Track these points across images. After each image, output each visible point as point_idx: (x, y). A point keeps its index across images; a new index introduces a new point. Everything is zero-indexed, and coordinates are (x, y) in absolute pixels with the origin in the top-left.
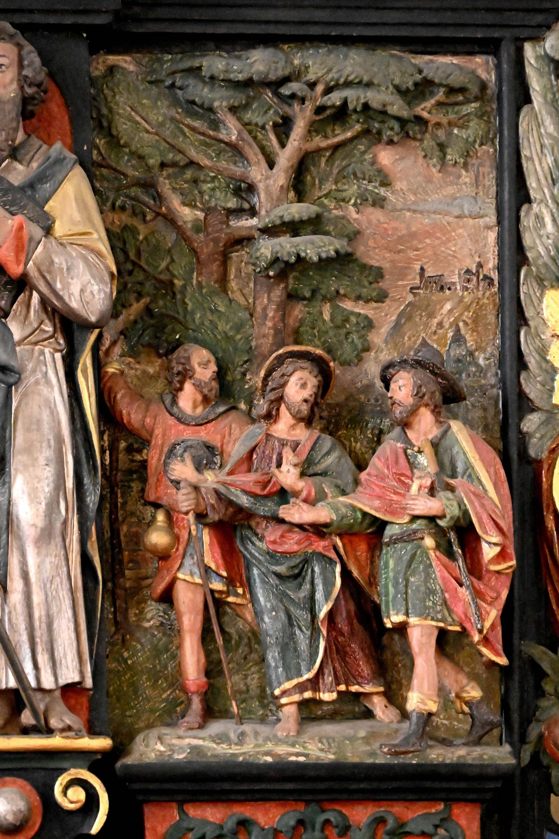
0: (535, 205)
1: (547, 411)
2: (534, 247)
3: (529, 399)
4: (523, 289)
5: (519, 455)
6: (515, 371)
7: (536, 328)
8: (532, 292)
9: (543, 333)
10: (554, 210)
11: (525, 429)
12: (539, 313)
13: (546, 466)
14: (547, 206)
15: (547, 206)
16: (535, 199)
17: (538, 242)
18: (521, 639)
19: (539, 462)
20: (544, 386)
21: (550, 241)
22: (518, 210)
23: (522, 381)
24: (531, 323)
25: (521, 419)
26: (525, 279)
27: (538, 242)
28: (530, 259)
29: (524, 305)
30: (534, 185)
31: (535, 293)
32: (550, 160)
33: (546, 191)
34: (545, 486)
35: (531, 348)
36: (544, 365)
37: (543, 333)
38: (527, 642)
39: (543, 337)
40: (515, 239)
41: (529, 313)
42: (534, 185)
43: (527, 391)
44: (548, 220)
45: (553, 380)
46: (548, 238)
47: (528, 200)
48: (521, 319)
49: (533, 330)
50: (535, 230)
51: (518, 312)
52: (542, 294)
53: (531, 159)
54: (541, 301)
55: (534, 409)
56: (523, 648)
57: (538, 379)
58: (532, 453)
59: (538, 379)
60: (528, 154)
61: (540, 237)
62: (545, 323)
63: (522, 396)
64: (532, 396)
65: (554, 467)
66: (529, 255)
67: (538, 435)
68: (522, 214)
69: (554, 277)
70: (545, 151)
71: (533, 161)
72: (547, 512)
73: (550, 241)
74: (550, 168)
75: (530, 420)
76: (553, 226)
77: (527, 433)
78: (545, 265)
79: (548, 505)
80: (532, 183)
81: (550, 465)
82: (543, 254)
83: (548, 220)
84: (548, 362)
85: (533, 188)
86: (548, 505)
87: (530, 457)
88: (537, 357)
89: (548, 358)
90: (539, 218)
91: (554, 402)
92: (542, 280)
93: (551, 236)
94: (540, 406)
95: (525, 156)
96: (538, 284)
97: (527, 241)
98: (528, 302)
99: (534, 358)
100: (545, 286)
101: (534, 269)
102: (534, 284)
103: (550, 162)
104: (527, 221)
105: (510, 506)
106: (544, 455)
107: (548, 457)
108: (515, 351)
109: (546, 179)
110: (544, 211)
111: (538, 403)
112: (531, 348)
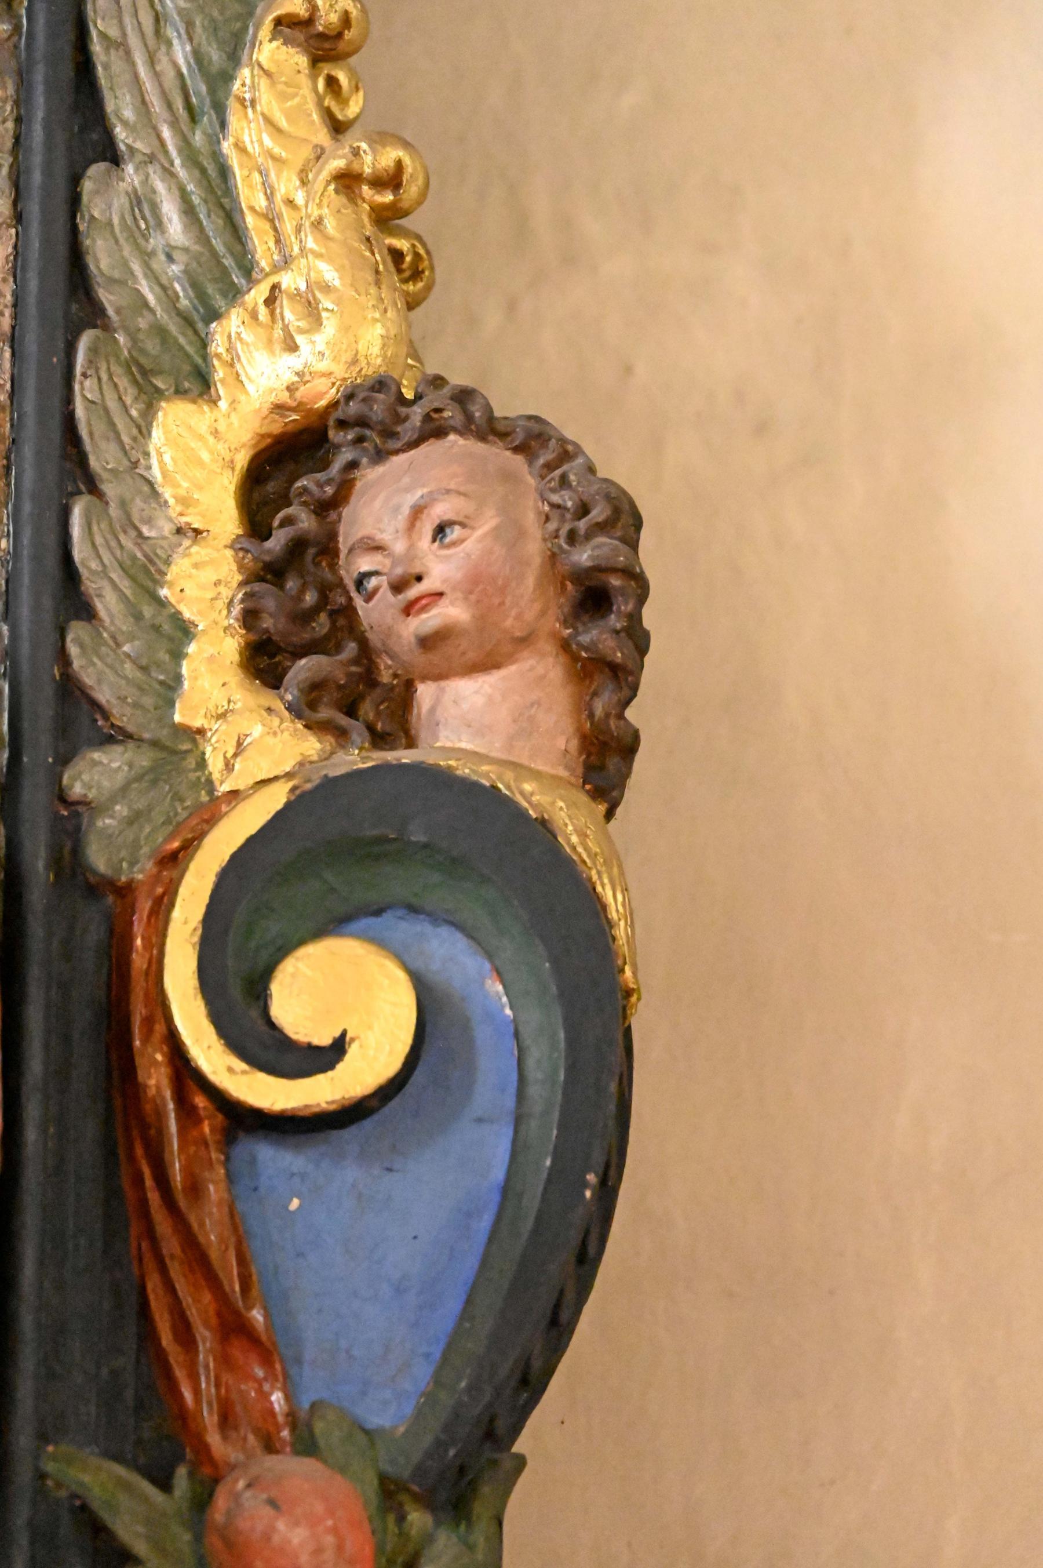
0: (130, 169)
1: (155, 744)
2: (123, 282)
3: (95, 705)
4: (85, 390)
5: (56, 862)
6: (48, 618)
7: (123, 504)
8: (112, 404)
9: (149, 521)
10: (190, 187)
11: (77, 790)
12: (135, 464)
13: (144, 906)
14: (169, 173)
15: (169, 173)
16: (131, 149)
17: (136, 267)
18: (43, 1437)
19: (125, 892)
20: (144, 669)
21: (175, 269)
22: (75, 180)
23: (73, 650)
24: (109, 489)
25: (64, 760)
26: (90, 362)
27: (136, 267)
28: (110, 312)
29: (83, 432)
30: (128, 114)
31: (126, 409)
32: (181, 53)
33: (166, 133)
34: (139, 961)
35: (107, 558)
36: (148, 611)
37: (149, 521)
38: (64, 1448)
39: (146, 531)
40: (62, 250)
41: (102, 457)
42: (128, 114)
43: (88, 679)
44: (170, 210)
45: (178, 656)
46: (170, 258)
47: (111, 155)
48: (74, 469)
49: (114, 511)
50: (132, 238)
51: (65, 457)
52: (149, 411)
53: (121, 45)
54: (143, 431)
55: (114, 736)
56: (50, 1467)
57: (126, 648)
58: (99, 858)
59: (126, 648)
60: (113, 32)
61: (147, 257)
62: (155, 494)
63: (70, 691)
64: (103, 695)
65: (172, 905)
66: (107, 298)
67: (121, 809)
68: (87, 186)
69: (187, 368)
70: (170, 33)
71: (128, 53)
72: (146, 1039)
73: (175, 269)
74: (180, 75)
75: (95, 763)
76: (186, 228)
77: (84, 802)
78: (160, 332)
79: (149, 1022)
80: (120, 107)
81: (158, 901)
82: (151, 299)
83: (170, 210)
84: (162, 604)
85: (125, 123)
86: (149, 1022)
87: (95, 873)
88: (125, 585)
89: (164, 592)
90: (141, 203)
91: (177, 718)
92: (145, 372)
93: (176, 255)
94: (131, 728)
95: (103, 36)
96: (135, 382)
97: (102, 256)
98: (100, 427)
99: (115, 586)
100: (158, 390)
101: (121, 338)
102: (123, 382)
103: (181, 61)
104: (105, 198)
105: (470, 1264)
106: (142, 872)
107: (156, 879)
108: (52, 561)
109: (169, 106)
110: (160, 186)
111: (123, 716)
112: (107, 558)
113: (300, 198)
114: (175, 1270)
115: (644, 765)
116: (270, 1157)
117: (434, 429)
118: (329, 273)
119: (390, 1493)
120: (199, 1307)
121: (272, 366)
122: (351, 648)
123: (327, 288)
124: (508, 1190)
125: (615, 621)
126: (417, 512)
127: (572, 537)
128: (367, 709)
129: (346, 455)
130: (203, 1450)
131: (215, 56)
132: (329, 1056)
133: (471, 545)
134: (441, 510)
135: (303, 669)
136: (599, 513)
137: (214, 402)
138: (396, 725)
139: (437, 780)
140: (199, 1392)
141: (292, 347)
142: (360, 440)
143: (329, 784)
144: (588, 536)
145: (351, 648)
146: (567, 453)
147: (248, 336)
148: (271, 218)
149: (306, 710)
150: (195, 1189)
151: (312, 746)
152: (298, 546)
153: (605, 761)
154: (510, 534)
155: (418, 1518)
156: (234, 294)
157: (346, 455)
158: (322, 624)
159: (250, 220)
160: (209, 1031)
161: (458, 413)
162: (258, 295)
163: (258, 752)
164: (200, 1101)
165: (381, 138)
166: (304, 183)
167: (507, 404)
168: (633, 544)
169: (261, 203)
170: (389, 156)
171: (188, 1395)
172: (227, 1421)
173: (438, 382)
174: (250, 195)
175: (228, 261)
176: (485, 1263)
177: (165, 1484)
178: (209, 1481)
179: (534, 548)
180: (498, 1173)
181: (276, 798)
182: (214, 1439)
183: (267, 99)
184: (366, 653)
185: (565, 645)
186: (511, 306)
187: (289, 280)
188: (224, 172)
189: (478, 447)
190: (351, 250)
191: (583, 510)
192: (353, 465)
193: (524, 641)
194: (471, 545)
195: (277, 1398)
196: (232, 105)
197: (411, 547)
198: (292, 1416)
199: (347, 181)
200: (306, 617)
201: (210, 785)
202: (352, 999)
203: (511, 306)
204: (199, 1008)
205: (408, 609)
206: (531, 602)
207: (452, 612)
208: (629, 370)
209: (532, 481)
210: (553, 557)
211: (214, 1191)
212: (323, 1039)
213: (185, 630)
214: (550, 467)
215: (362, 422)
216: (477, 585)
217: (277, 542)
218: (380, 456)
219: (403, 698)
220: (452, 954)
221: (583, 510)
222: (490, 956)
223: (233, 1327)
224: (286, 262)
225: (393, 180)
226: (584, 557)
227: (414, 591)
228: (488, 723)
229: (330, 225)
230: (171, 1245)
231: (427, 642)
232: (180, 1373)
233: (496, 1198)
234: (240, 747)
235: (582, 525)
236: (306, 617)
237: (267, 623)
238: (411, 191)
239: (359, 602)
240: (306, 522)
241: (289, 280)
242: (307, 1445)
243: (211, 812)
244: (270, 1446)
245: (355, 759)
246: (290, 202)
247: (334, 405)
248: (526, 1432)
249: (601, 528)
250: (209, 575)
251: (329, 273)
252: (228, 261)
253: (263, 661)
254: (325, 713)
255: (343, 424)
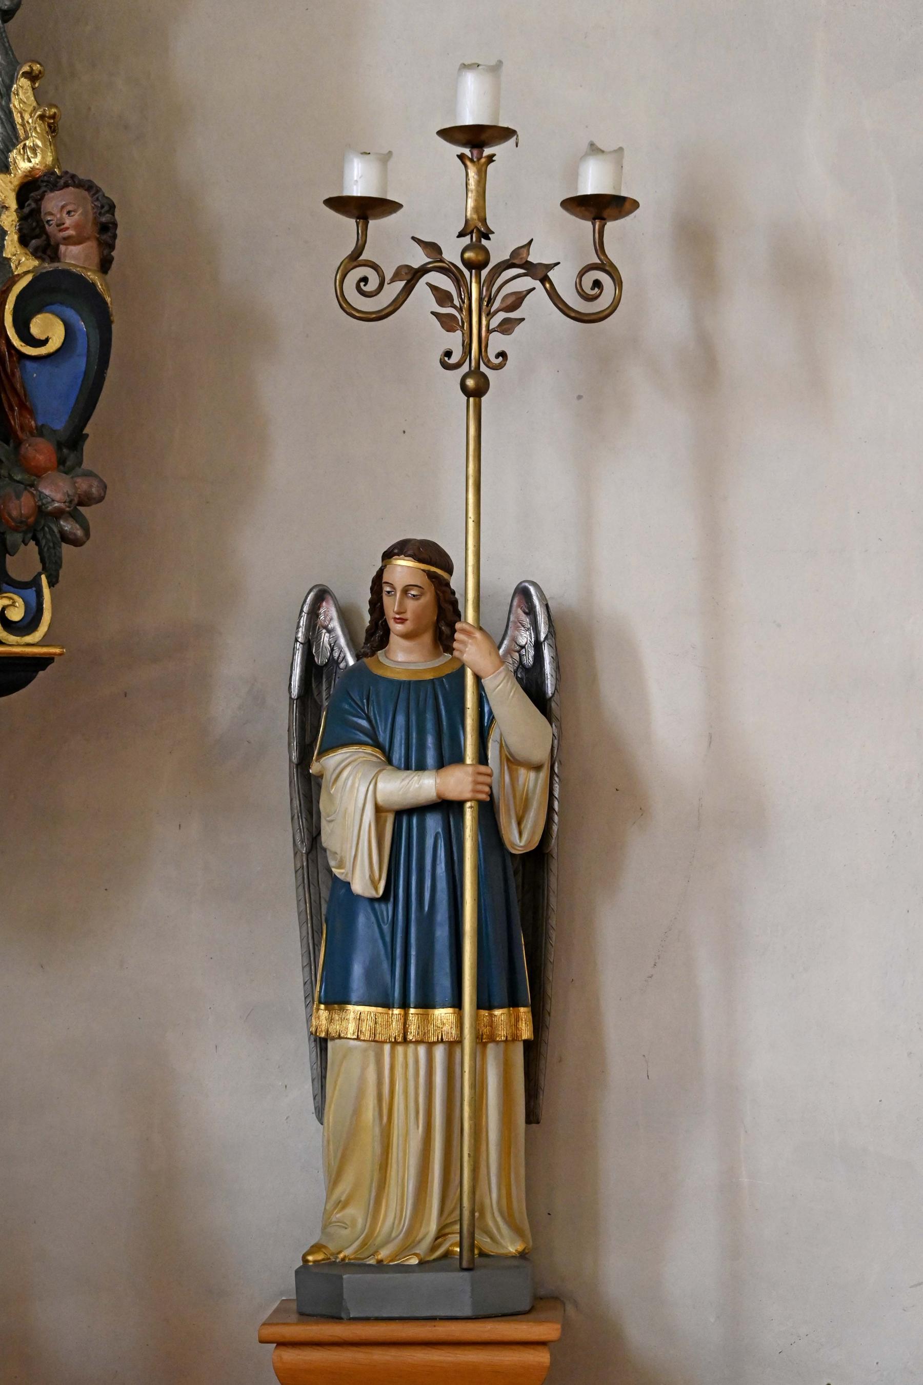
113: (30, 121)
114: (8, 392)
115: (114, 265)
116: (29, 365)
117: (66, 185)
118: (39, 144)
119: (59, 446)
120: (14, 401)
121: (24, 164)
122: (44, 237)
123: (38, 147)
124: (85, 373)
125: (109, 234)
126: (63, 207)
127: (100, 214)
128: (49, 252)
129: (43, 189)
130: (17, 436)
131: (7, 81)
132: (45, 342)
133: (76, 217)
134: (69, 208)
135: (34, 242)
136: (106, 208)
137: (10, 174)
138: (55, 257)
139: (67, 273)
140: (15, 423)
141: (30, 161)
142: (46, 186)
143: (42, 274)
144: (104, 214)
145: (44, 237)
146: (98, 190)
147: (19, 158)
148: (23, 125)
149: (35, 254)
150: (13, 374)
151: (36, 263)
152: (32, 211)
153: (105, 265)
154: (85, 213)
155: (65, 451)
156: (14, 146)
157: (43, 189)
158: (37, 231)
159: (18, 127)
160: (16, 336)
161: (72, 181)
162: (20, 146)
163: (23, 263)
164: (13, 352)
165: (51, 106)
166: (31, 117)
167: (82, 175)
168: (113, 215)
169: (20, 121)
170: (53, 110)
171: (12, 422)
172: (22, 428)
173: (66, 173)
174: (18, 119)
175: (12, 137)
176: (81, 390)
177: (7, 443)
178: (19, 443)
179: (91, 216)
180: (83, 369)
181: (28, 279)
182: (19, 433)
183: (21, 96)
184: (48, 237)
185: (98, 239)
186: (57, 89)
187: (27, 142)
188: (11, 112)
189: (77, 190)
190: (44, 137)
191: (102, 207)
192: (45, 192)
193: (88, 239)
194: (76, 217)
195: (33, 423)
196: (12, 95)
197: (61, 215)
198: (36, 427)
199: (42, 117)
200: (33, 229)
201: (12, 273)
202: (50, 329)
203: (57, 89)
204: (13, 330)
205: (60, 231)
206: (90, 229)
207: (71, 232)
208: (90, 109)
209: (89, 198)
210: (95, 218)
211: (18, 374)
212: (43, 338)
213: (5, 233)
214: (94, 194)
215: (47, 181)
216: (77, 226)
217: (26, 210)
218: (52, 190)
219: (56, 248)
220: (71, 314)
221: (102, 207)
222: (80, 315)
223: (22, 406)
224: (27, 138)
225: (53, 117)
226: (103, 219)
227: (62, 227)
228: (76, 257)
229: (38, 129)
230: (7, 387)
231: (64, 239)
232: (11, 417)
233: (82, 374)
234: (19, 263)
235: (103, 211)
236: (33, 229)
237: (25, 231)
238: (57, 119)
239: (47, 226)
240: (33, 205)
241: (27, 142)
242: (41, 435)
243: (14, 280)
244: (32, 435)
245: (48, 267)
246: (28, 122)
247: (40, 177)
248: (88, 426)
249: (107, 212)
250: (10, 219)
251: (39, 144)
252: (12, 137)
253: (24, 241)
254: (39, 254)
255: (42, 181)
